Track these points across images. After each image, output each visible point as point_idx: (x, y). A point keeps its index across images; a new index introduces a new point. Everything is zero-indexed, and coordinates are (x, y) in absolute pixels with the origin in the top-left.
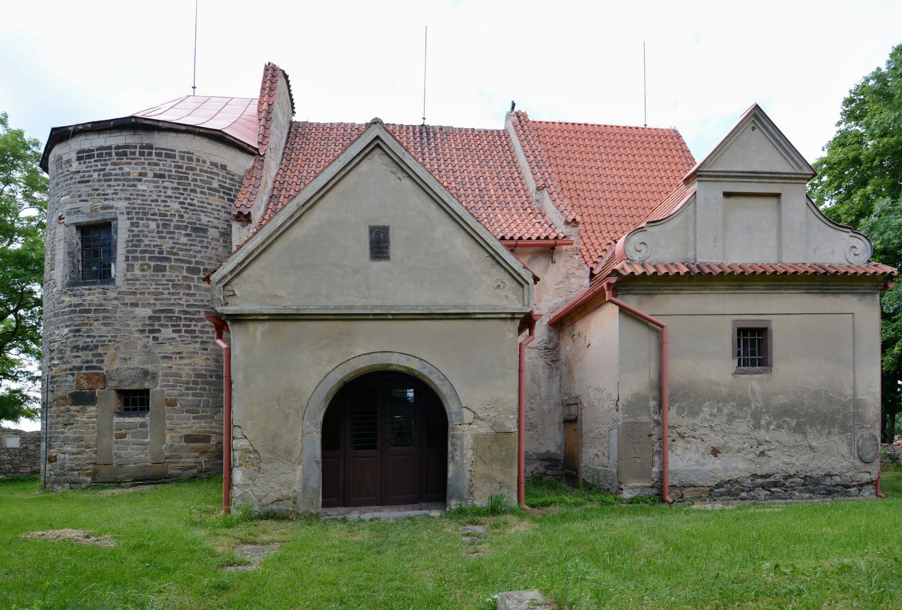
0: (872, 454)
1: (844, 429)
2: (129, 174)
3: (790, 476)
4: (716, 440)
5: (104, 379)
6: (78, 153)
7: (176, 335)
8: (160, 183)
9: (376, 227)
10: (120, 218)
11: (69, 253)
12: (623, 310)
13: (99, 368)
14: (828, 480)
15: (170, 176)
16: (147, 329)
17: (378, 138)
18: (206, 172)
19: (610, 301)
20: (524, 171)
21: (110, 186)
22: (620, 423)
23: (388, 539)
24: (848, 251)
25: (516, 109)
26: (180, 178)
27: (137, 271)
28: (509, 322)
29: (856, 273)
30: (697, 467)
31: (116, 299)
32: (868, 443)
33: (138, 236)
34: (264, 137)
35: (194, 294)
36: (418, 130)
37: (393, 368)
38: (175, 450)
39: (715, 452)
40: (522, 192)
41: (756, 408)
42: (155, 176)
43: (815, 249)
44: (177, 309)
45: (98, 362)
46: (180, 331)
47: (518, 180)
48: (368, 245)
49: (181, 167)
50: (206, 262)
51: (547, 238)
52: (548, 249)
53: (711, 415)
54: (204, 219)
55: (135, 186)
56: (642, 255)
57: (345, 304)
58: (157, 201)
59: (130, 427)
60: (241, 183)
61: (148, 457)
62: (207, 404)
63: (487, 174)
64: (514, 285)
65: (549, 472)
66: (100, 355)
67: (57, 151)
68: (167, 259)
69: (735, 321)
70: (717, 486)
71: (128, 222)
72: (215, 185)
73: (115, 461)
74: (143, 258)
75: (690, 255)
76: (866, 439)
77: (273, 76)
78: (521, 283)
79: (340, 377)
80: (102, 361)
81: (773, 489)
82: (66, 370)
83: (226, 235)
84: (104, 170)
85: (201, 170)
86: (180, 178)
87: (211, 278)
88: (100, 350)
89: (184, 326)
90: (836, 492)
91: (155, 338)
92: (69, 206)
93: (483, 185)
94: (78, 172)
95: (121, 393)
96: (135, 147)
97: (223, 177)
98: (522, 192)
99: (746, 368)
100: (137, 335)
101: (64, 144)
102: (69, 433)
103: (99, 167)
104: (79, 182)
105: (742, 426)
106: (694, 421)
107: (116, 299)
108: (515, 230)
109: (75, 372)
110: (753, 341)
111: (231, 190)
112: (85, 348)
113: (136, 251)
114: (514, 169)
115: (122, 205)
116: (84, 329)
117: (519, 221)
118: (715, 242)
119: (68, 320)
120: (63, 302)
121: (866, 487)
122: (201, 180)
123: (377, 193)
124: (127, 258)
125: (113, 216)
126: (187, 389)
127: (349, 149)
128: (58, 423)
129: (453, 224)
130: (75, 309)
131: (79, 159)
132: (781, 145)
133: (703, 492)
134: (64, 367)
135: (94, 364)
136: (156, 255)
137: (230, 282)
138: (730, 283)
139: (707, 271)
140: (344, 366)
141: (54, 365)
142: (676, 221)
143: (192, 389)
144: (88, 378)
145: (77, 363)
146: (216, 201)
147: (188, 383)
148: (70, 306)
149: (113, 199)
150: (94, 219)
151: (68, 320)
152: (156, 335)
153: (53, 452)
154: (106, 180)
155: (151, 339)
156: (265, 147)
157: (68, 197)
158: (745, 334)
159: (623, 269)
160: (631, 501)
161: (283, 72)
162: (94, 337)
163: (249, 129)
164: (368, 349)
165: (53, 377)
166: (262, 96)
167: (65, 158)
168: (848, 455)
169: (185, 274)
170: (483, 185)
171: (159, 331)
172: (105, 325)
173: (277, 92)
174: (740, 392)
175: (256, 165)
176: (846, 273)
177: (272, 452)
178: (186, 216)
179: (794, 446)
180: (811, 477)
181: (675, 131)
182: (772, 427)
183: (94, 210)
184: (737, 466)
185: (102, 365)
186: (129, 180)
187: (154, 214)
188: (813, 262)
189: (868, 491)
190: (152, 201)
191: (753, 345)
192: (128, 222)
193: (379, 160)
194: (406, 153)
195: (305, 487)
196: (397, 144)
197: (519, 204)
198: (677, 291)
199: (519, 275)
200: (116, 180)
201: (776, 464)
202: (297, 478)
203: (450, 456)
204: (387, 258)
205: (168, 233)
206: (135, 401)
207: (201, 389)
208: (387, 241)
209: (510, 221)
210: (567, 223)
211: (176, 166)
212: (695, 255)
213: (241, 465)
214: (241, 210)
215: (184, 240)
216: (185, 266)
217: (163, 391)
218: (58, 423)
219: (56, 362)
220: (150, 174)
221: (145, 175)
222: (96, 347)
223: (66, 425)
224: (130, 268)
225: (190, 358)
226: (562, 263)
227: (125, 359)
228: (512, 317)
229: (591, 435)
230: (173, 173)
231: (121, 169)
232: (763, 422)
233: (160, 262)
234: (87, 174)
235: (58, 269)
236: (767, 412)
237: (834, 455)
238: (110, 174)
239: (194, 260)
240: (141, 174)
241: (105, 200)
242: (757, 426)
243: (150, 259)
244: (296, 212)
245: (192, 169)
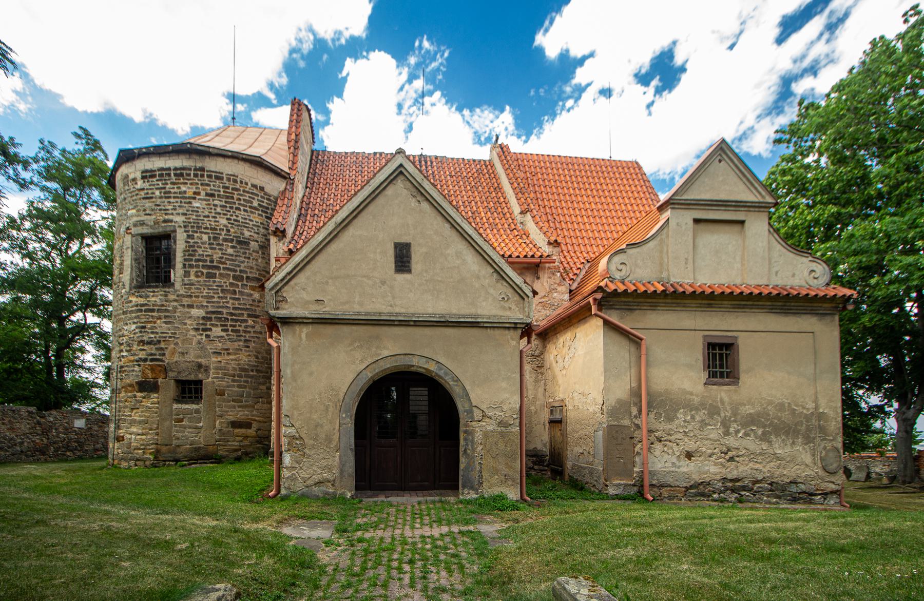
0: (835, 465)
1: (808, 440)
2: (185, 192)
3: (757, 482)
4: (691, 446)
5: (165, 370)
6: (143, 172)
7: (224, 334)
8: (211, 202)
10: (178, 230)
11: (136, 260)
12: (607, 323)
13: (161, 360)
14: (793, 486)
15: (219, 196)
16: (201, 327)
17: (401, 165)
18: (248, 192)
19: (596, 315)
20: (508, 197)
21: (169, 202)
22: (605, 426)
23: (411, 523)
24: (804, 274)
25: (499, 142)
26: (227, 197)
27: (192, 277)
28: (512, 331)
29: (816, 295)
30: (673, 469)
31: (175, 300)
32: (831, 454)
33: (193, 246)
34: (294, 163)
35: (239, 299)
36: (417, 158)
37: (412, 369)
38: (224, 434)
39: (689, 455)
40: (508, 215)
41: (725, 416)
42: (207, 195)
43: (777, 273)
44: (225, 311)
45: (160, 355)
46: (227, 330)
47: (504, 205)
48: (392, 259)
49: (228, 188)
50: (248, 270)
51: (533, 256)
52: (532, 267)
53: (685, 421)
54: (247, 234)
55: (190, 203)
56: (623, 273)
57: (374, 311)
58: (208, 216)
59: (190, 412)
60: (276, 203)
61: (202, 440)
62: (249, 395)
63: (478, 198)
64: (517, 298)
65: (536, 467)
66: (162, 349)
67: (124, 170)
68: (218, 268)
69: (705, 336)
70: (691, 487)
71: (185, 234)
72: (255, 204)
73: (175, 442)
74: (198, 266)
75: (664, 275)
76: (829, 450)
77: (299, 110)
78: (522, 297)
79: (370, 375)
80: (164, 355)
81: (743, 493)
82: (133, 361)
83: (265, 247)
84: (164, 188)
85: (244, 191)
86: (227, 197)
87: (266, 285)
88: (162, 345)
89: (231, 326)
90: (801, 499)
91: (208, 336)
92: (135, 219)
93: (475, 208)
94: (143, 189)
95: (179, 382)
96: (190, 169)
98: (508, 215)
99: (715, 380)
100: (192, 333)
101: (130, 164)
102: (136, 416)
103: (161, 186)
104: (144, 198)
105: (714, 432)
106: (670, 427)
107: (175, 300)
108: (506, 249)
109: (142, 363)
110: (721, 355)
111: (268, 208)
112: (149, 343)
113: (191, 260)
114: (500, 194)
115: (180, 219)
116: (149, 326)
117: (507, 241)
118: (686, 263)
119: (135, 318)
120: (131, 302)
121: (829, 496)
122: (244, 200)
123: (399, 216)
124: (184, 265)
125: (172, 228)
126: (233, 381)
128: (127, 407)
129: (464, 242)
130: (140, 308)
131: (143, 178)
132: (745, 176)
133: (680, 492)
134: (132, 358)
135: (158, 357)
136: (208, 263)
137: (280, 289)
138: (700, 302)
139: (681, 290)
140: (374, 365)
141: (123, 356)
142: (651, 244)
143: (237, 381)
144: (152, 369)
145: (142, 355)
146: (256, 218)
147: (234, 375)
148: (137, 306)
149: (172, 214)
150: (156, 231)
151: (135, 318)
152: (209, 333)
153: (121, 432)
154: (166, 198)
155: (204, 337)
156: (294, 172)
157: (134, 211)
158: (714, 349)
159: (606, 286)
160: (617, 497)
162: (157, 333)
164: (391, 351)
165: (122, 367)
166: (290, 127)
167: (131, 177)
168: (811, 465)
169: (231, 281)
170: (475, 208)
171: (210, 330)
172: (166, 323)
173: (302, 124)
174: (710, 402)
176: (807, 295)
177: (315, 439)
178: (232, 230)
179: (760, 454)
180: (777, 483)
181: (637, 163)
182: (740, 435)
183: (156, 222)
184: (710, 469)
185: (163, 358)
186: (186, 198)
187: (206, 228)
189: (832, 500)
190: (205, 217)
191: (721, 359)
192: (185, 234)
195: (342, 472)
197: (506, 226)
198: (654, 307)
199: (520, 288)
200: (174, 197)
201: (743, 470)
202: (336, 463)
203: (462, 449)
204: (409, 271)
205: (217, 245)
206: (189, 390)
207: (245, 382)
208: (409, 256)
209: (500, 240)
210: (549, 243)
211: (224, 187)
213: (289, 450)
214: (279, 226)
215: (230, 251)
216: (232, 274)
217: (214, 383)
218: (127, 407)
219: (125, 354)
220: (203, 193)
221: (199, 194)
222: (159, 342)
223: (132, 409)
224: (187, 274)
225: (235, 354)
226: (545, 280)
227: (183, 353)
228: (515, 326)
229: (576, 435)
230: (222, 193)
231: (179, 188)
232: (732, 430)
233: (211, 269)
234: (150, 192)
235: (125, 274)
236: (735, 421)
237: (800, 462)
238: (170, 192)
239: (238, 269)
240: (195, 193)
241: (166, 214)
242: (727, 433)
243: (204, 267)
244: (334, 230)
245: (237, 190)
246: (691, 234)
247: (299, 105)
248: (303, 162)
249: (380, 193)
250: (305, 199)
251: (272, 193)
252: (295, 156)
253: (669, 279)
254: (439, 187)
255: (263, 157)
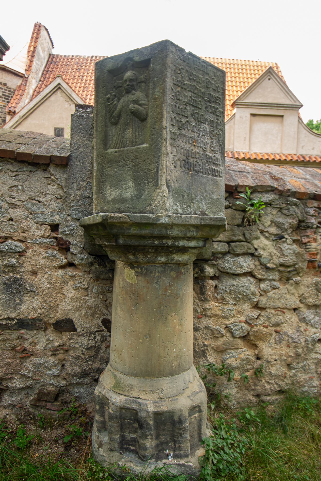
9: (58, 128)
17: (59, 84)
43: (303, 147)
60: (14, 93)
97: (5, 90)
111: (9, 97)
118: (245, 140)
127: (45, 89)
132: (284, 89)
161: (45, 27)
163: (22, 62)
175: (23, 83)
188: (301, 153)
193: (60, 95)
194: (73, 92)
196: (68, 87)
212: (234, 147)
244: (19, 120)
246: (248, 123)
247: (40, 26)
248: (39, 65)
249: (47, 99)
250: (37, 89)
251: (12, 87)
252: (31, 61)
253: (233, 149)
254: (80, 95)
255: (6, 65)
